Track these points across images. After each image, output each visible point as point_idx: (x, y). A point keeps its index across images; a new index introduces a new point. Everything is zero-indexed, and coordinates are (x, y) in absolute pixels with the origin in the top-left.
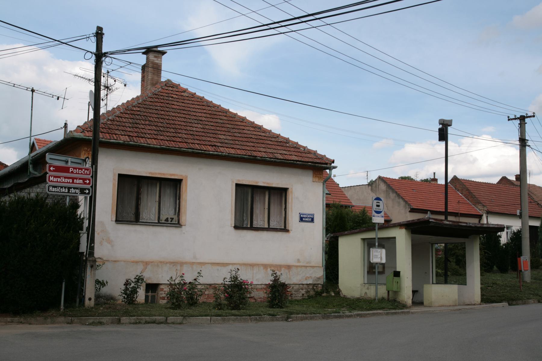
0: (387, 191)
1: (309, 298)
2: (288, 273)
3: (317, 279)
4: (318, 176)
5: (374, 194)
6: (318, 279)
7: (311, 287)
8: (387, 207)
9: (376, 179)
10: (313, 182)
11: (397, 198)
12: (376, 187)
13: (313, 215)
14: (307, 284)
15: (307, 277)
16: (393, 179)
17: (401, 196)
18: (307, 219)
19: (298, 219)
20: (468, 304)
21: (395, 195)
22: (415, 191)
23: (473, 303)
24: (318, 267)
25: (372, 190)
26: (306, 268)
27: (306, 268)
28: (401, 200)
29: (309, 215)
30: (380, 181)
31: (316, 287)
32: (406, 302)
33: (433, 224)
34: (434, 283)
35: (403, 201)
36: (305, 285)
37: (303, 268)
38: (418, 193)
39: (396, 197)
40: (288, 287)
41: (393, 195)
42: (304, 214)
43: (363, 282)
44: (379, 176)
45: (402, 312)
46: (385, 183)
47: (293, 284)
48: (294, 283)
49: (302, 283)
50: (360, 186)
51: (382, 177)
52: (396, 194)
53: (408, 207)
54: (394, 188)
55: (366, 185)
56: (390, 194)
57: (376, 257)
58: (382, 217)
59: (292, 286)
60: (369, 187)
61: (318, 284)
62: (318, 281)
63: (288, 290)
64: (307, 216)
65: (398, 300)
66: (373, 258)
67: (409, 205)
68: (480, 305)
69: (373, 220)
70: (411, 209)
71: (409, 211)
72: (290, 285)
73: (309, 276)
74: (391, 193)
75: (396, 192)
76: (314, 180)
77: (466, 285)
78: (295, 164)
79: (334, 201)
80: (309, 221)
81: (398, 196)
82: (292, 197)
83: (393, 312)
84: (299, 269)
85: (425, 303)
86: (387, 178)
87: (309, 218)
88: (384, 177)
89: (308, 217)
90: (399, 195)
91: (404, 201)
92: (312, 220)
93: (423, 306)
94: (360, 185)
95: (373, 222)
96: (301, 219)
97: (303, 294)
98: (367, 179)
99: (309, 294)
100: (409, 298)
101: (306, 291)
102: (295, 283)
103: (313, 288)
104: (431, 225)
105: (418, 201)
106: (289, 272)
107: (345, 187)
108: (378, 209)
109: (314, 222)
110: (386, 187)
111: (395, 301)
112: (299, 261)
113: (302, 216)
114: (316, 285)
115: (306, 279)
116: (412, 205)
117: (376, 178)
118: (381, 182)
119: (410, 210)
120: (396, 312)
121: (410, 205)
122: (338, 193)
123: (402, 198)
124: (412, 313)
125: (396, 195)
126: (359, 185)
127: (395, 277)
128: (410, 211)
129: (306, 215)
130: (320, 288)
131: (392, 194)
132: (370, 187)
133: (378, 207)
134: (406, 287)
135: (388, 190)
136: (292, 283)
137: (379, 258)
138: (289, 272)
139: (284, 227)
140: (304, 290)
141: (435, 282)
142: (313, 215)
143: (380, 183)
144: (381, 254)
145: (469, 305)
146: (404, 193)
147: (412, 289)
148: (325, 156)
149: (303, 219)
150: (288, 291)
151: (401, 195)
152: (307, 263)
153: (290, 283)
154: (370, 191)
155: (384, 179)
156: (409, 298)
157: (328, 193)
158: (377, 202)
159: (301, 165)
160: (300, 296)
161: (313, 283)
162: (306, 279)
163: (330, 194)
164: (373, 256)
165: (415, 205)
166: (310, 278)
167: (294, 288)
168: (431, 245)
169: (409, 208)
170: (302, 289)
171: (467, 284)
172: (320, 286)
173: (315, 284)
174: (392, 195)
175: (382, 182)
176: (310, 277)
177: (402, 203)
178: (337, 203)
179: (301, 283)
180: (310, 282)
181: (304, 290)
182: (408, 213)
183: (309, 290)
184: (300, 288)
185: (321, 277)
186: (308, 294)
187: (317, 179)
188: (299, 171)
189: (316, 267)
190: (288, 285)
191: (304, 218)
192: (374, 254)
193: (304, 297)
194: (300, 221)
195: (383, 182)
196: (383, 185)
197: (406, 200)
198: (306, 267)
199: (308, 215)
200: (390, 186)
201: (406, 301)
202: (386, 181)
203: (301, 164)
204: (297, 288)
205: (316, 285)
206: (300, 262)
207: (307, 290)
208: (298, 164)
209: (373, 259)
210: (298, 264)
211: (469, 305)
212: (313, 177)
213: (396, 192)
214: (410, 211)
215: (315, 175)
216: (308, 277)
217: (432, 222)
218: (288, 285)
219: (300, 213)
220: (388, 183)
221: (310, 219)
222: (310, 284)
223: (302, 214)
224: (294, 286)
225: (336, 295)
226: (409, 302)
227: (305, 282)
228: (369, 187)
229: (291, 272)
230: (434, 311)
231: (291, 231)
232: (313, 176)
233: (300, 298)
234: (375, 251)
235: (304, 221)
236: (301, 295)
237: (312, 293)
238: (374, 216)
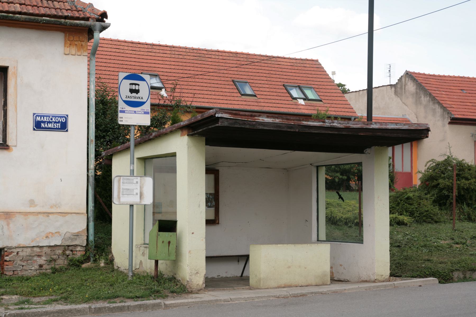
0: (417, 93)
1: (54, 273)
2: (6, 227)
3: (73, 237)
4: (76, 43)
5: (399, 98)
6: (75, 237)
7: (59, 251)
8: (417, 118)
9: (402, 76)
10: (66, 54)
11: (431, 103)
12: (401, 88)
13: (66, 117)
14: (50, 247)
15: (50, 233)
16: (431, 75)
17: (437, 100)
18: (50, 125)
19: (31, 124)
20: (365, 279)
21: (428, 98)
22: (465, 91)
23: (373, 278)
24: (74, 214)
25: (396, 93)
26: (48, 216)
27: (48, 216)
28: (437, 106)
29: (56, 117)
30: (407, 79)
31: (72, 251)
32: (188, 281)
33: (226, 124)
34: (320, 239)
35: (440, 108)
36: (45, 248)
37: (41, 216)
38: (470, 95)
39: (429, 101)
40: (6, 253)
41: (426, 99)
42: (44, 116)
43: (143, 242)
44: (406, 71)
45: (140, 307)
46: (414, 81)
47: (16, 248)
48: (20, 244)
49: (37, 245)
50: (380, 88)
51: (410, 73)
52: (430, 97)
53: (447, 116)
54: (427, 88)
55: (388, 85)
56: (421, 97)
57: (129, 192)
58: (146, 113)
59: (16, 251)
60: (391, 88)
61: (76, 246)
62: (76, 239)
63: (7, 258)
64: (52, 119)
65: (178, 278)
66: (121, 195)
67: (448, 113)
68: (389, 281)
69: (119, 119)
70: (451, 120)
71: (448, 123)
72: (10, 248)
73: (54, 232)
74: (423, 97)
75: (430, 95)
76: (67, 52)
77: (363, 243)
78: (12, 19)
79: (318, 110)
80: (56, 129)
81: (432, 100)
82: (16, 83)
83: (114, 307)
84: (31, 218)
85: (252, 281)
86: (419, 74)
87: (55, 122)
88: (414, 73)
89: (54, 120)
90: (434, 99)
91: (441, 107)
92: (64, 127)
93: (247, 287)
94: (379, 87)
95: (120, 123)
96: (38, 126)
97: (41, 266)
98: (390, 76)
99: (55, 265)
100: (197, 273)
101: (49, 259)
102: (21, 246)
103: (64, 253)
104: (220, 124)
105: (466, 107)
106: (8, 225)
107: (360, 91)
108: (134, 98)
109: (67, 131)
110: (415, 87)
111: (173, 279)
112: (32, 203)
113: (38, 119)
114: (70, 248)
115: (47, 237)
116: (453, 113)
117: (402, 75)
118: (409, 80)
119: (449, 121)
120: (124, 307)
121: (451, 113)
122: (334, 98)
123: (439, 103)
124: (166, 306)
125: (430, 99)
126: (377, 86)
127: (161, 233)
128: (450, 123)
129: (49, 117)
130: (79, 254)
131: (424, 97)
132: (393, 89)
133: (134, 94)
134: (190, 252)
135: (418, 91)
136: (14, 245)
137: (137, 194)
138: (8, 225)
139: (3, 141)
140: (44, 258)
141: (323, 236)
142: (66, 117)
143: (407, 81)
144: (141, 188)
145: (366, 281)
146: (444, 96)
147: (206, 255)
148: (91, 5)
149: (43, 125)
150: (6, 261)
151: (437, 98)
152: (51, 207)
153: (10, 246)
154: (393, 95)
155: (414, 75)
156: (197, 273)
157: (319, 98)
158: (132, 84)
159: (25, 21)
160: (33, 268)
161: (63, 244)
162: (47, 237)
163: (321, 101)
164: (121, 191)
165: (459, 113)
166: (56, 235)
167: (21, 254)
168: (314, 170)
169: (448, 118)
170: (39, 256)
171: (364, 243)
172: (79, 249)
173: (68, 246)
174: (425, 99)
175: (410, 80)
176: (56, 233)
177: (439, 110)
178: (323, 112)
179: (35, 245)
180: (58, 242)
181: (44, 258)
182: (447, 126)
183: (55, 257)
184: (33, 255)
185: (82, 231)
186: (53, 266)
187: (73, 50)
188: (33, 34)
189: (71, 213)
190: (6, 250)
191: (44, 122)
192: (122, 187)
193: (44, 271)
194: (34, 130)
195: (411, 79)
196: (412, 84)
197: (445, 105)
198: (47, 214)
199: (53, 116)
200: (421, 86)
201: (188, 280)
202: (416, 78)
203: (26, 18)
204: (27, 254)
205: (70, 248)
206: (36, 206)
207: (51, 258)
208: (18, 20)
209: (119, 198)
210: (32, 210)
211: (366, 281)
212: (65, 46)
213: (430, 95)
214: (450, 123)
215: (69, 42)
216: (52, 233)
217: (221, 118)
218: (6, 250)
219: (34, 114)
220: (420, 81)
221: (59, 125)
222: (56, 246)
223: (39, 116)
224: (19, 250)
225: (107, 266)
226: (199, 281)
227: (45, 243)
228: (391, 88)
229: (11, 225)
230: (229, 301)
231: (13, 148)
232: (65, 44)
233: (35, 273)
234: (125, 181)
235: (43, 128)
236: (37, 267)
237: (62, 262)
238: (123, 112)
